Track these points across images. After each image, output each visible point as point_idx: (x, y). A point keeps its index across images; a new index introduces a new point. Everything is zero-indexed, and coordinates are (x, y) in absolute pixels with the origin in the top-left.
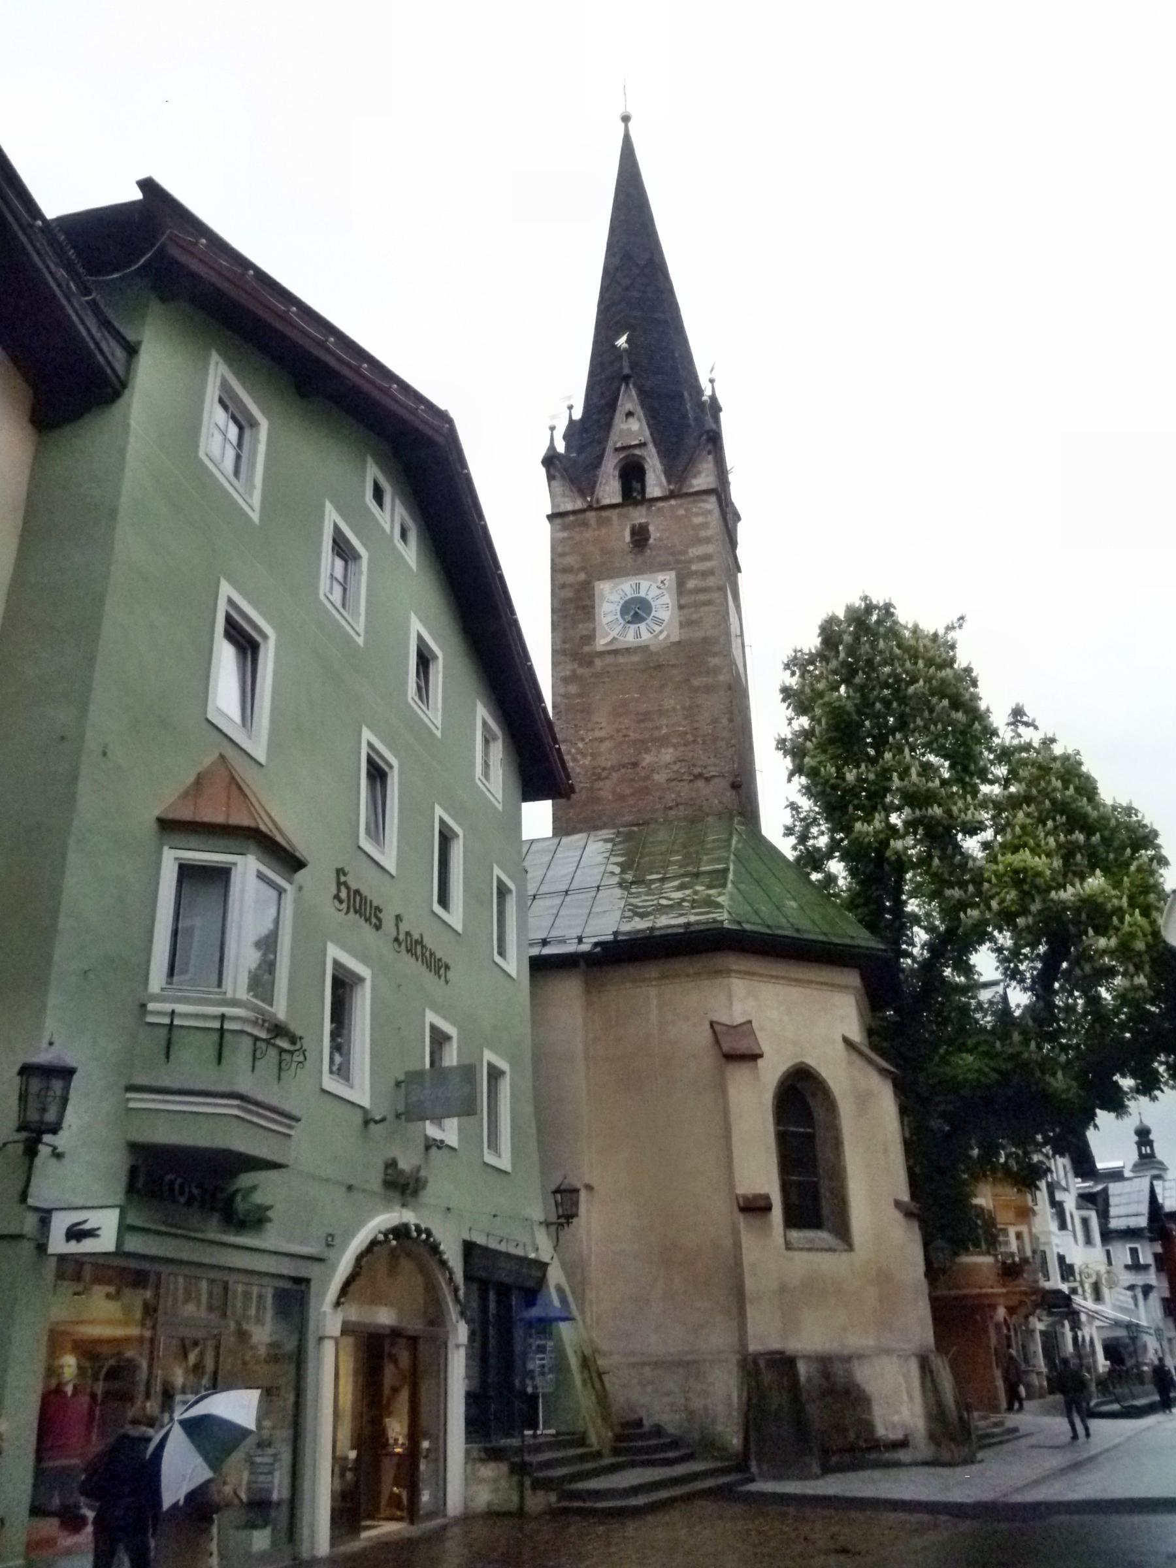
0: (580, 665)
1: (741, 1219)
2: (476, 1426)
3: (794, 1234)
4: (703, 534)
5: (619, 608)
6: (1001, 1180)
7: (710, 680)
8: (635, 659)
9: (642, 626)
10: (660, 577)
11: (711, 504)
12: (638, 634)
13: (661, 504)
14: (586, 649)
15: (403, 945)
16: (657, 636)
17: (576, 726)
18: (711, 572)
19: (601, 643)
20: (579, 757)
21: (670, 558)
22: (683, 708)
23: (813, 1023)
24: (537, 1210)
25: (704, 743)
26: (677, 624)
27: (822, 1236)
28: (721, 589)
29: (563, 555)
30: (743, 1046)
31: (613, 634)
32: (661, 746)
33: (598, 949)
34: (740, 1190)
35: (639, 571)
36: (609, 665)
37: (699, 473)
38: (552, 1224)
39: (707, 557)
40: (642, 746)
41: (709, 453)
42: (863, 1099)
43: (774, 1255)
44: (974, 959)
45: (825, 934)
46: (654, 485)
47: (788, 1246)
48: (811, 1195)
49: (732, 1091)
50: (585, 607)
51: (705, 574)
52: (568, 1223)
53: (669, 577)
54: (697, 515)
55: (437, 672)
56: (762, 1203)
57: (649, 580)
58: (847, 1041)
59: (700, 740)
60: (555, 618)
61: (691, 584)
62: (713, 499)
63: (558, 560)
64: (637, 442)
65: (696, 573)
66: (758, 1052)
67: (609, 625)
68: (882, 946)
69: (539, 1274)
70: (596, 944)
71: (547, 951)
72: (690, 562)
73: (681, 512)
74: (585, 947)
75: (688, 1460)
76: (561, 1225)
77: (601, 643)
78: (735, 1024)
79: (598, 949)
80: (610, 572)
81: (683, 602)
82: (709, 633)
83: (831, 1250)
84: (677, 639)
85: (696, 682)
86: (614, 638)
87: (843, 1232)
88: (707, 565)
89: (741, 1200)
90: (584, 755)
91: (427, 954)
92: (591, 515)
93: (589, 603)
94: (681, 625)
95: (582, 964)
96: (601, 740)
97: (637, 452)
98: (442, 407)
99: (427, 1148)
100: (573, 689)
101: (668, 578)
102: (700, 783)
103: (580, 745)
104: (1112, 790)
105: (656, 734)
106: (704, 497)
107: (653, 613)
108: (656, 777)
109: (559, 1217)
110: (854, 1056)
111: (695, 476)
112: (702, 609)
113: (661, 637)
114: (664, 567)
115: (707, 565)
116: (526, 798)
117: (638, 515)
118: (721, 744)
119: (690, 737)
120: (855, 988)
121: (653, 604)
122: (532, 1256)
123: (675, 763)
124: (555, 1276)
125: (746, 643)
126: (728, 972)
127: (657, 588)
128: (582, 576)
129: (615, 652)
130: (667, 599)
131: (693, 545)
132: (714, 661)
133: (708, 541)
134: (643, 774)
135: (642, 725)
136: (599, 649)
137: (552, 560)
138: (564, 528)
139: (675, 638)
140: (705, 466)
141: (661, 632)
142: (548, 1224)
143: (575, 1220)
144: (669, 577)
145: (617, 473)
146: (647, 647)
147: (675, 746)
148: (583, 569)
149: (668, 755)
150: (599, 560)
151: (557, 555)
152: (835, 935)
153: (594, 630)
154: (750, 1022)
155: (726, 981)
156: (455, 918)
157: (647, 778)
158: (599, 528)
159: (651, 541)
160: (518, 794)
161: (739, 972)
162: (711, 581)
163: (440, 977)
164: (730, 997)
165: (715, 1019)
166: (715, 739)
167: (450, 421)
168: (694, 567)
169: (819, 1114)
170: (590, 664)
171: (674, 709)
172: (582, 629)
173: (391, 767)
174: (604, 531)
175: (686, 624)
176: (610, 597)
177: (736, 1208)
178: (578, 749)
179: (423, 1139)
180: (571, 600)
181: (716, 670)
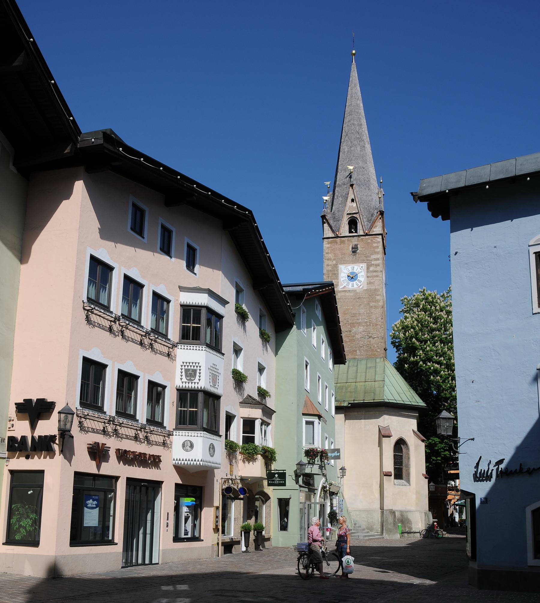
12: (353, 286)
30: (386, 433)
37: (376, 226)
48: (399, 472)
53: (364, 265)
54: (375, 243)
58: (413, 431)
61: (371, 269)
65: (373, 265)
97: (355, 215)
102: (371, 339)
113: (361, 287)
117: (355, 241)
128: (334, 262)
130: (363, 274)
133: (378, 253)
144: (364, 265)
145: (347, 223)
159: (358, 251)
168: (373, 263)
169: (404, 450)
174: (342, 245)
175: (369, 283)
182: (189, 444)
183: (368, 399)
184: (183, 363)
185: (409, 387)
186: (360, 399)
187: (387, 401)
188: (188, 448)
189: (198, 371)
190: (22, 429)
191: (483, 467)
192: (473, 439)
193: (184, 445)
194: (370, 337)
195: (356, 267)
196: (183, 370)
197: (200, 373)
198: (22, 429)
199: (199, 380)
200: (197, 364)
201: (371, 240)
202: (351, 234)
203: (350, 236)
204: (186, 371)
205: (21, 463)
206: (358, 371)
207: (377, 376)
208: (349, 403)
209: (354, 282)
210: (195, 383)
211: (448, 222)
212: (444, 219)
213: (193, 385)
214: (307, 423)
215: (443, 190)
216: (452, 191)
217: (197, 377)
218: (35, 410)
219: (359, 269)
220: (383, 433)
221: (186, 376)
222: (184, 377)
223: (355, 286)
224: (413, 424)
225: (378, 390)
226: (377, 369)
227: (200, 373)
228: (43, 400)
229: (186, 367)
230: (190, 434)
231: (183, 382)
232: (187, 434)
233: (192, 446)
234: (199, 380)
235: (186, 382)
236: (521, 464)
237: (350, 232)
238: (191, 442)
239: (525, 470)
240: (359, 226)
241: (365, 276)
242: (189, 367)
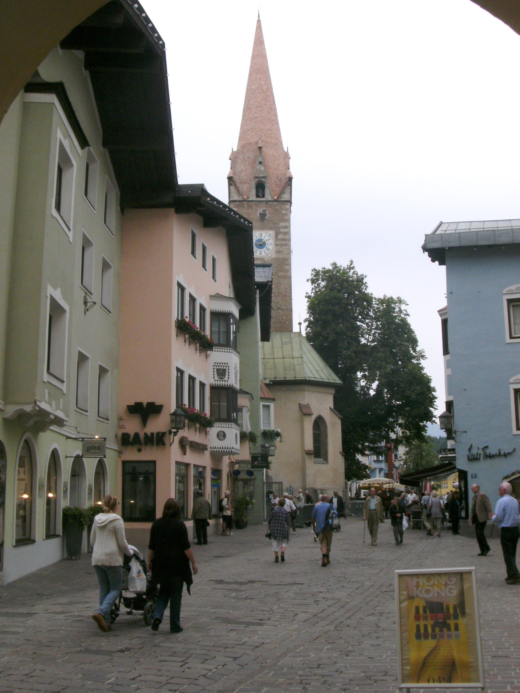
12: (261, 253)
16: (267, 255)
23: (323, 404)
27: (321, 460)
30: (308, 411)
43: (313, 467)
44: (258, 279)
48: (319, 451)
53: (272, 233)
54: (283, 209)
58: (330, 408)
61: (280, 237)
65: (282, 232)
72: (280, 228)
73: (278, 208)
75: (417, 630)
85: (280, 274)
87: (326, 459)
94: (276, 252)
97: (263, 180)
102: (280, 311)
104: (412, 327)
106: (286, 203)
107: (266, 246)
113: (269, 255)
114: (271, 229)
126: (304, 390)
130: (271, 241)
131: (281, 222)
139: (274, 257)
144: (272, 233)
145: (255, 187)
158: (248, 209)
159: (266, 217)
164: (304, 396)
168: (281, 230)
169: (322, 428)
174: (250, 210)
175: (278, 252)
177: (304, 453)
182: (222, 434)
183: (290, 377)
184: (215, 363)
185: (325, 364)
186: (281, 377)
187: (308, 379)
188: (221, 437)
189: (227, 371)
190: (133, 426)
191: (474, 451)
192: (466, 432)
193: (218, 435)
194: (279, 308)
195: (264, 234)
196: (215, 370)
197: (229, 372)
198: (133, 426)
199: (228, 378)
200: (226, 365)
201: (280, 207)
202: (258, 199)
203: (258, 201)
204: (218, 370)
205: (132, 455)
206: (275, 346)
207: (294, 352)
208: (271, 381)
209: (262, 250)
210: (225, 381)
211: (444, 267)
212: (440, 264)
213: (224, 383)
214: (264, 406)
215: (444, 246)
216: (450, 248)
217: (227, 376)
218: (145, 411)
219: (267, 236)
220: (304, 411)
221: (218, 375)
222: (216, 375)
223: (263, 254)
224: (330, 403)
225: (297, 367)
226: (294, 345)
227: (229, 372)
228: (154, 403)
229: (218, 367)
230: (223, 426)
231: (215, 380)
232: (220, 426)
233: (224, 436)
234: (228, 378)
235: (217, 380)
236: (499, 450)
237: (258, 196)
238: (224, 432)
239: (502, 453)
240: (267, 192)
241: (273, 244)
242: (220, 367)
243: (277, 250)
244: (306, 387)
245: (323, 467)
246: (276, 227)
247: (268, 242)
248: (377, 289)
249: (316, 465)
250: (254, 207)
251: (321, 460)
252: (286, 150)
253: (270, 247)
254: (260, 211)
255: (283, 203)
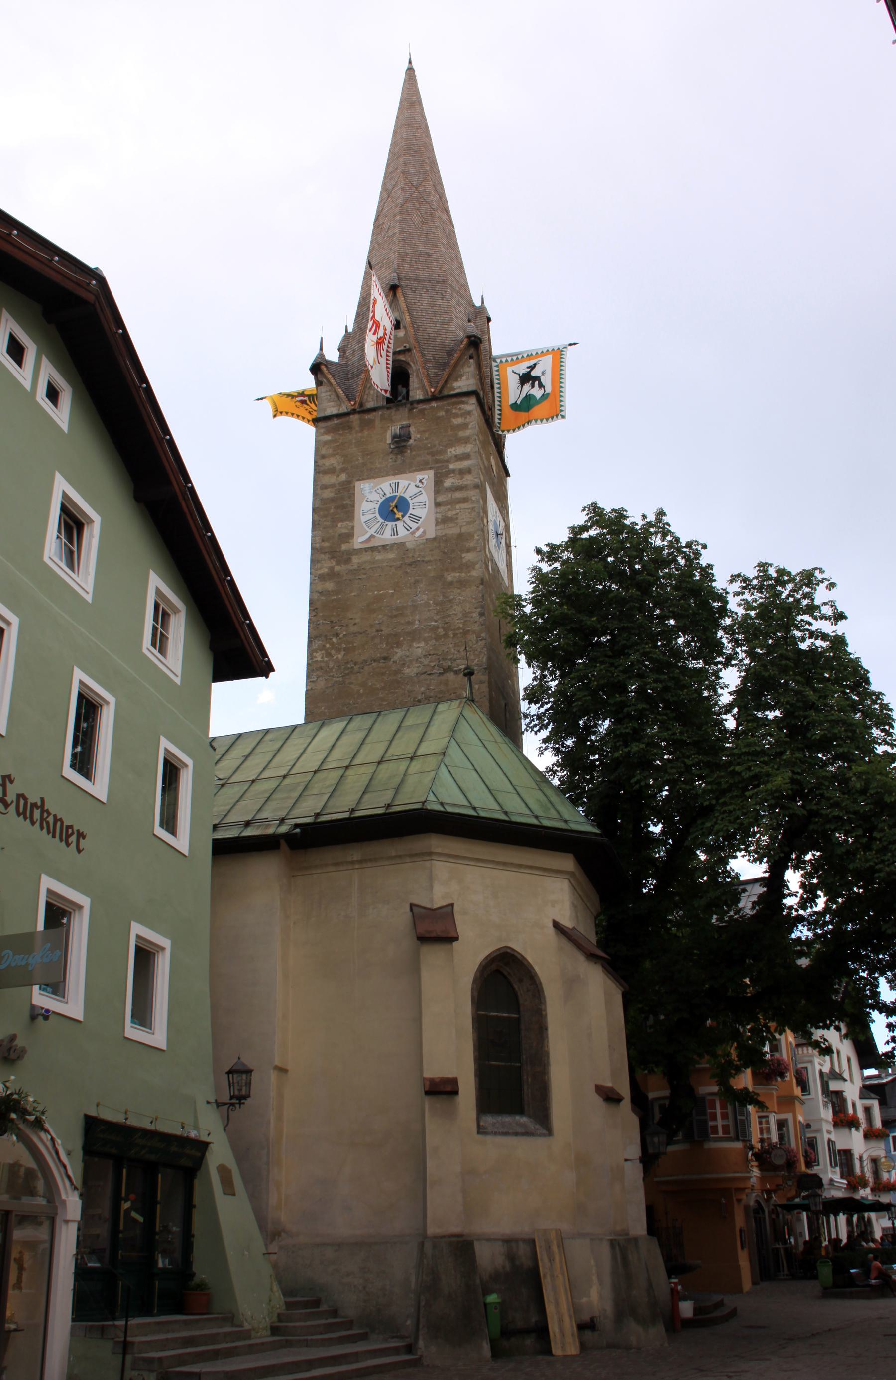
0: (338, 563)
1: (427, 1101)
2: (84, 1307)
3: (488, 1120)
4: (461, 434)
5: (377, 507)
6: (735, 1074)
7: (463, 575)
8: (391, 556)
9: (400, 524)
10: (419, 476)
11: (471, 405)
12: (395, 532)
13: (421, 406)
14: (344, 547)
15: (13, 808)
17: (332, 622)
18: (469, 471)
19: (359, 541)
20: (333, 652)
21: (429, 458)
22: (436, 604)
23: (531, 910)
24: (203, 1089)
25: (455, 635)
26: (433, 523)
28: (480, 487)
29: (323, 457)
30: (438, 929)
31: (372, 532)
32: (413, 640)
33: (298, 830)
34: (427, 1074)
35: (399, 470)
36: (365, 562)
37: (461, 376)
38: (225, 1104)
39: (466, 456)
40: (394, 641)
41: (471, 357)
42: (571, 983)
43: (459, 1141)
45: (536, 817)
46: (418, 389)
47: (481, 1130)
48: (510, 1078)
49: (425, 974)
50: (344, 507)
51: (462, 472)
52: (240, 1104)
53: (428, 476)
54: (456, 416)
55: (92, 537)
56: (449, 1088)
57: (406, 479)
58: (556, 925)
59: (451, 634)
60: (316, 518)
61: (448, 482)
62: (473, 400)
63: (320, 462)
64: (402, 348)
65: (454, 471)
66: (453, 934)
67: (368, 525)
68: (597, 831)
69: (199, 1154)
70: (296, 826)
71: (249, 832)
73: (442, 414)
74: (284, 829)
76: (233, 1104)
77: (359, 541)
78: (435, 907)
79: (298, 830)
80: (372, 473)
81: (439, 499)
82: (463, 530)
83: (527, 1134)
84: (433, 536)
85: (450, 577)
86: (372, 536)
88: (466, 463)
89: (427, 1083)
90: (338, 651)
91: (51, 819)
92: (355, 418)
93: (348, 502)
94: (437, 523)
95: (283, 844)
96: (355, 634)
98: (92, 265)
99: (33, 1018)
100: (329, 585)
101: (426, 476)
103: (334, 640)
105: (409, 628)
106: (464, 399)
107: (411, 511)
108: (407, 671)
109: (232, 1098)
110: (565, 942)
111: (456, 380)
112: (458, 507)
113: (418, 534)
114: (422, 467)
115: (466, 463)
116: (220, 675)
118: (473, 638)
119: (441, 632)
120: (572, 874)
121: (411, 502)
122: (193, 1134)
123: (425, 656)
124: (220, 1154)
125: (513, 544)
126: (429, 854)
127: (416, 487)
128: (343, 477)
129: (373, 549)
130: (424, 497)
132: (468, 557)
133: (466, 440)
134: (394, 668)
135: (395, 620)
136: (357, 546)
137: (315, 462)
138: (334, 430)
139: (431, 534)
140: (467, 369)
141: (418, 529)
142: (219, 1104)
143: (248, 1102)
144: (428, 476)
146: (403, 544)
147: (426, 641)
148: (343, 470)
149: (419, 648)
150: (361, 461)
151: (319, 456)
152: (549, 819)
153: (353, 527)
154: (452, 905)
155: (428, 863)
156: (99, 787)
157: (397, 672)
158: (362, 431)
159: (411, 441)
160: (208, 670)
161: (440, 854)
162: (468, 479)
163: (68, 844)
164: (431, 878)
165: (416, 902)
166: (466, 633)
167: (102, 282)
168: (451, 466)
170: (348, 561)
171: (427, 604)
172: (342, 528)
173: (9, 623)
174: (366, 433)
175: (443, 521)
176: (370, 495)
178: (332, 644)
179: (29, 1005)
180: (332, 500)
181: (470, 566)
201: (447, 411)
223: (402, 532)
243: (439, 516)
244: (436, 843)
245: (524, 1149)
246: (437, 461)
247: (415, 500)
248: (731, 556)
249: (489, 1139)
250: (378, 423)
251: (524, 1119)
252: (478, 304)
253: (422, 513)
254: (395, 429)
255: (454, 400)
